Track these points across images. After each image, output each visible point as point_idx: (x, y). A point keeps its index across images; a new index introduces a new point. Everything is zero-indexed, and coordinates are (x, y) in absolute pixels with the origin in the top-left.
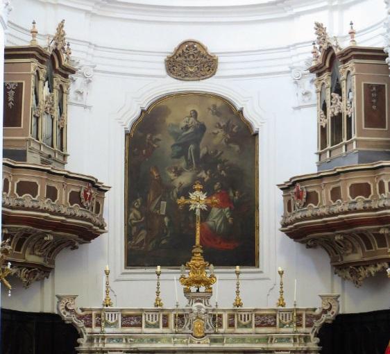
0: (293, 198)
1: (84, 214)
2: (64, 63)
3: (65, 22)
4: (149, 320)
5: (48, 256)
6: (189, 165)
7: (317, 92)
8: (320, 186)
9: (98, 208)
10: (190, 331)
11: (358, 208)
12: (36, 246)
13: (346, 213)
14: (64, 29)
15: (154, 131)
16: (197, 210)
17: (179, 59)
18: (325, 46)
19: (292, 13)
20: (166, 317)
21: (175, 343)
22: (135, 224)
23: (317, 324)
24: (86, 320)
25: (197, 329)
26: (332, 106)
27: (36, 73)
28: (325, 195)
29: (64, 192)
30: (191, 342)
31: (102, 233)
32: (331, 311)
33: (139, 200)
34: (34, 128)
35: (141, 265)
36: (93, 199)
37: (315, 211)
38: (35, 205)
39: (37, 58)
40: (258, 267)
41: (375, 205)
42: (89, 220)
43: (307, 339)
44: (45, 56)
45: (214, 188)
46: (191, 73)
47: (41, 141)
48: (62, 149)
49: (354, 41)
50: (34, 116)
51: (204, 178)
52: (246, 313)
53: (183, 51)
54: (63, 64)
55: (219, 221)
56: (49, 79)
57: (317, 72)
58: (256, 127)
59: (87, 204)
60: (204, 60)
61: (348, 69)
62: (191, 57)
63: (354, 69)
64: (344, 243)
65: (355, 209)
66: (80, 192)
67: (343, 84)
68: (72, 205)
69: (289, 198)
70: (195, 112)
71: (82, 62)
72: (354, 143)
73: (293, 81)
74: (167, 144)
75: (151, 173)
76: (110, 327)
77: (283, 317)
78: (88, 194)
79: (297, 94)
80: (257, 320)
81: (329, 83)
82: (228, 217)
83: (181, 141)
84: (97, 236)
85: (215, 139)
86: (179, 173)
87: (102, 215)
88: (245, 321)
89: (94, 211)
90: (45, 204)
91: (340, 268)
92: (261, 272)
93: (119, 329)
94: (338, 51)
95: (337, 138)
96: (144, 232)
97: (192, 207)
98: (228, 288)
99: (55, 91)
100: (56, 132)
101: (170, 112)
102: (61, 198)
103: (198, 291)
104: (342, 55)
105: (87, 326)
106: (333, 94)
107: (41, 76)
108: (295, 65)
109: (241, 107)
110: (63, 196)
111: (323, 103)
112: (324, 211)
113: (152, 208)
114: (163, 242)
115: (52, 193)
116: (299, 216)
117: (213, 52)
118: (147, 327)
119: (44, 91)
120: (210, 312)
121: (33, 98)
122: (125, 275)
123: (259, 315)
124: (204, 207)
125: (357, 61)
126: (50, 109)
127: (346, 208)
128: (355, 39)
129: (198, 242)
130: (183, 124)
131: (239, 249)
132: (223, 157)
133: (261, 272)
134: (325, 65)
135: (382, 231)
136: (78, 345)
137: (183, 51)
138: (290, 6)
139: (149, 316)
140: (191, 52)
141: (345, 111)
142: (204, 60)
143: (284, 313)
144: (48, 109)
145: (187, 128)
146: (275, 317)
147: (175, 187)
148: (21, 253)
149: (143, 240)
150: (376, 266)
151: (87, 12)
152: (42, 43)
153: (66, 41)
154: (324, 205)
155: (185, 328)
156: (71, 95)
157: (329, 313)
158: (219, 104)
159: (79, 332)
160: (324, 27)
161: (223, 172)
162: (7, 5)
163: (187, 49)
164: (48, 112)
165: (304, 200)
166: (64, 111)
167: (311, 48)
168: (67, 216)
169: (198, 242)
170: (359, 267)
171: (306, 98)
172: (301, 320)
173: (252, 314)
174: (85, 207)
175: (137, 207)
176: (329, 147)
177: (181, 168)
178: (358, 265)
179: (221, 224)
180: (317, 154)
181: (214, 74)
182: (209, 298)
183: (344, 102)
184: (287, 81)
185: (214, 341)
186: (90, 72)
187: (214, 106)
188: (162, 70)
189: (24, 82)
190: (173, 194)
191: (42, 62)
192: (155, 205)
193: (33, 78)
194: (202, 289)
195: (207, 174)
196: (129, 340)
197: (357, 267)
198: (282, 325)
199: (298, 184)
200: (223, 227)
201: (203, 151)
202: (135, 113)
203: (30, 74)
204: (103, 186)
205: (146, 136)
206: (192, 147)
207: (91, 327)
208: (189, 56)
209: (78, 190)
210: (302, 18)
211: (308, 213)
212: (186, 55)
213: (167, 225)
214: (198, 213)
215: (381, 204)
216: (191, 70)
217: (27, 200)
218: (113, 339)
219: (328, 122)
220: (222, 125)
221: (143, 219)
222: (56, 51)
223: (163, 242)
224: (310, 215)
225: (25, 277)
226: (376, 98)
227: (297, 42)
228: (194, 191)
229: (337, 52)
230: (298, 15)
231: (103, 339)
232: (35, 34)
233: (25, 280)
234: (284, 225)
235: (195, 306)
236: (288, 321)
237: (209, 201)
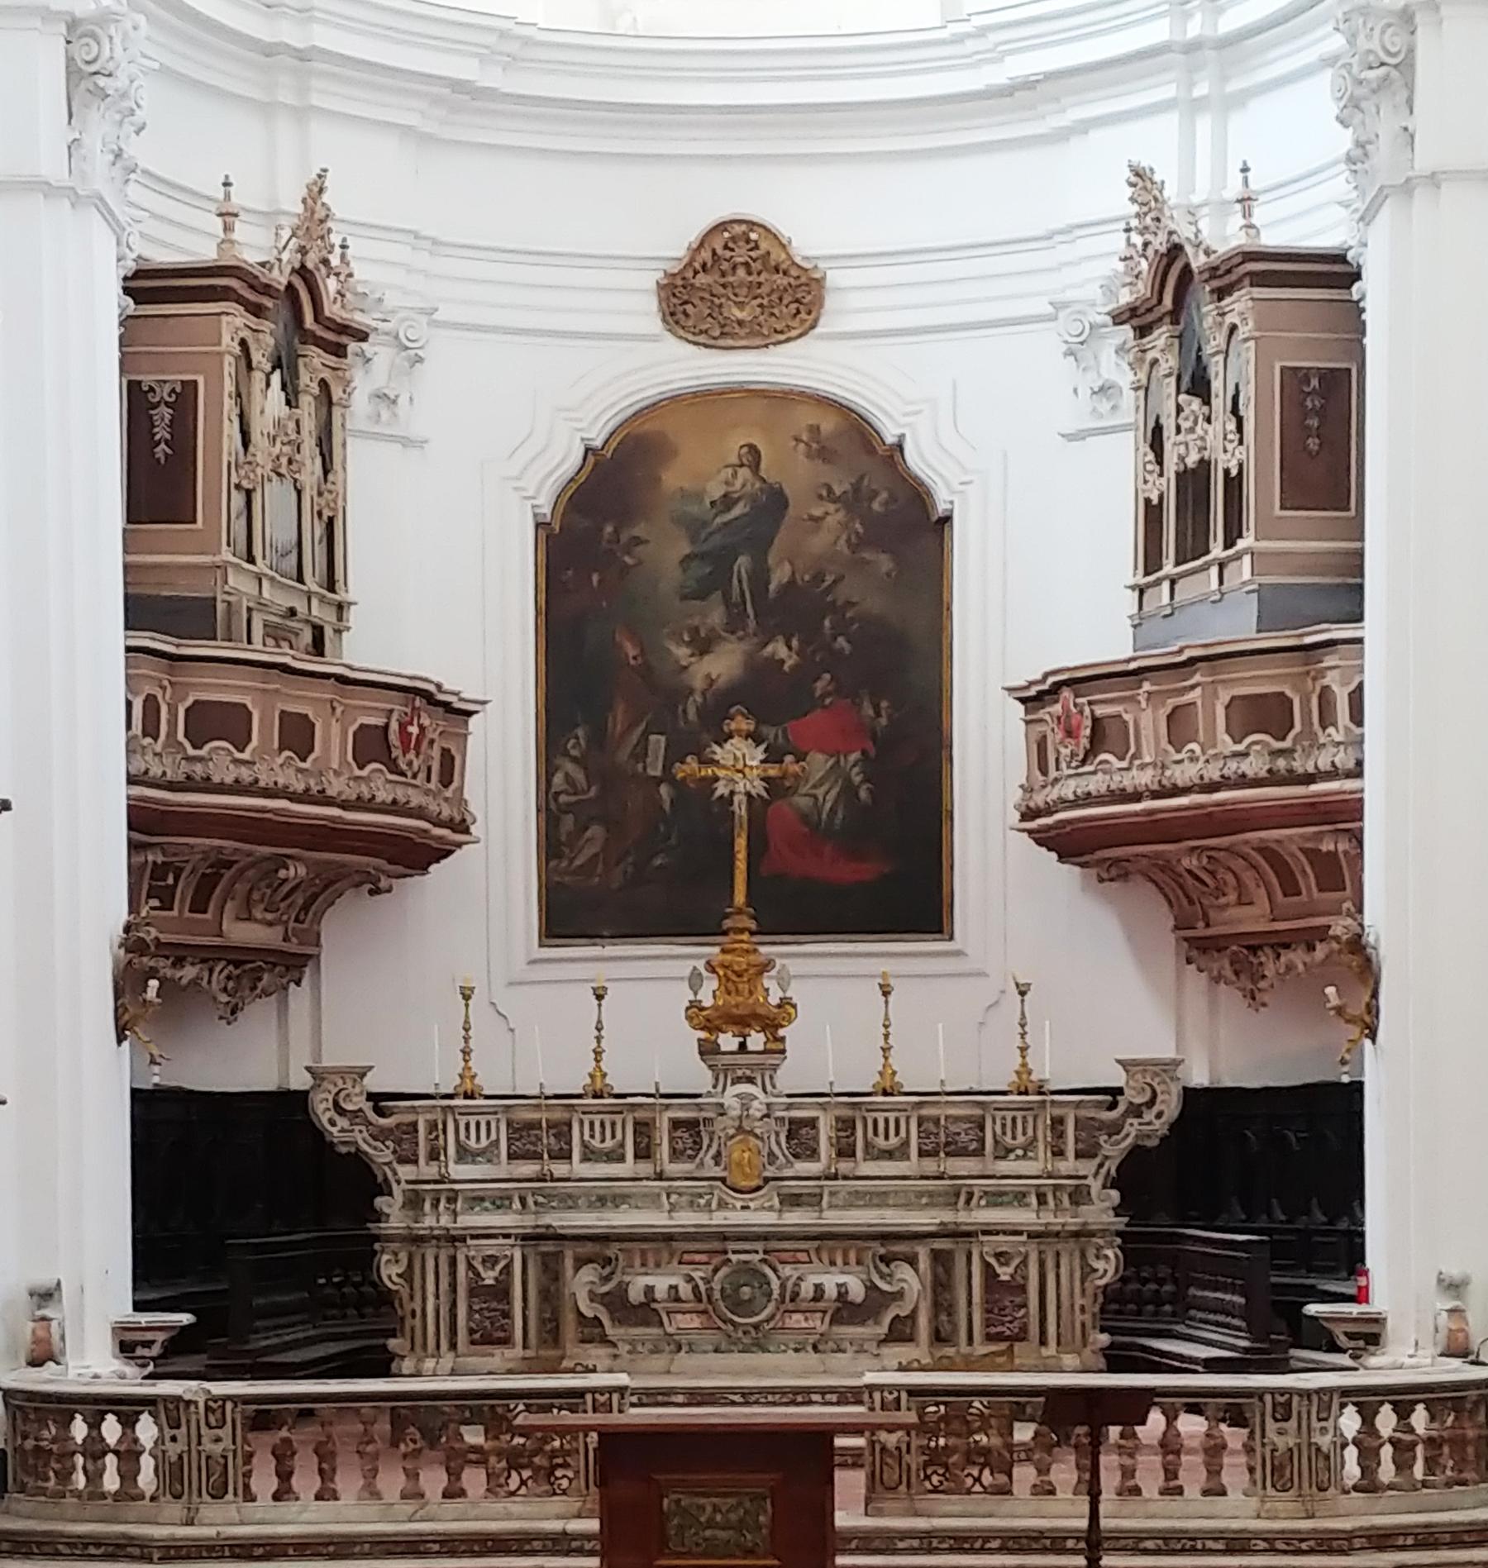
0: (1055, 736)
1: (400, 794)
2: (331, 310)
3: (329, 174)
4: (592, 1136)
5: (297, 920)
6: (735, 624)
7: (1136, 389)
8: (1133, 699)
9: (449, 769)
10: (718, 1172)
11: (1250, 773)
12: (256, 896)
13: (1212, 787)
14: (326, 198)
15: (625, 515)
16: (736, 799)
17: (702, 279)
18: (1160, 243)
19: (1063, 123)
20: (643, 1129)
21: (673, 1208)
22: (568, 809)
23: (1114, 1151)
24: (398, 1142)
25: (739, 1164)
26: (1181, 438)
27: (237, 350)
28: (1147, 721)
29: (336, 728)
30: (723, 1205)
31: (459, 845)
32: (1155, 1110)
33: (580, 732)
34: (240, 526)
35: (591, 935)
36: (432, 742)
37: (1117, 778)
38: (245, 774)
39: (240, 300)
40: (951, 938)
41: (1301, 765)
42: (419, 813)
43: (1079, 1196)
44: (267, 290)
45: (813, 691)
46: (740, 323)
47: (261, 566)
48: (331, 586)
49: (1250, 226)
50: (238, 487)
51: (783, 662)
52: (892, 1116)
53: (714, 253)
54: (327, 313)
55: (829, 796)
56: (285, 363)
57: (1136, 322)
58: (942, 500)
59: (410, 764)
60: (781, 281)
61: (1230, 319)
62: (741, 272)
63: (1251, 324)
64: (1212, 874)
65: (1244, 775)
66: (386, 727)
67: (1215, 366)
68: (361, 767)
69: (1040, 728)
70: (753, 449)
71: (392, 300)
72: (1247, 559)
73: (1064, 347)
74: (666, 553)
75: (620, 647)
76: (474, 1162)
77: (1004, 1126)
78: (414, 730)
79: (1075, 391)
80: (923, 1134)
81: (1169, 362)
82: (857, 779)
83: (705, 547)
84: (449, 853)
85: (816, 536)
86: (703, 646)
87: (461, 788)
88: (887, 1137)
89: (434, 777)
90: (279, 770)
91: (1201, 946)
92: (958, 953)
93: (503, 1169)
94: (1202, 259)
95: (1193, 547)
96: (595, 831)
97: (721, 789)
98: (843, 1013)
99: (306, 401)
100: (313, 531)
101: (675, 453)
102: (344, 733)
103: (743, 1046)
104: (1213, 272)
105: (402, 1161)
106: (1183, 397)
107: (257, 357)
108: (1070, 295)
109: (898, 432)
110: (333, 741)
111: (1151, 424)
112: (1144, 778)
113: (623, 755)
114: (658, 862)
115: (297, 735)
116: (1068, 790)
117: (810, 253)
118: (585, 1159)
119: (270, 403)
120: (779, 1114)
121: (232, 430)
122: (537, 967)
123: (929, 1119)
124: (758, 788)
125: (1258, 292)
126: (290, 462)
127: (1213, 773)
128: (1254, 221)
129: (740, 898)
130: (716, 491)
131: (894, 883)
132: (843, 593)
133: (958, 953)
134: (1160, 301)
135: (1327, 846)
136: (379, 1216)
137: (714, 253)
138: (1057, 100)
139: (592, 1124)
140: (741, 255)
141: (1222, 457)
142: (781, 281)
143: (1009, 1115)
144: (284, 460)
145: (728, 501)
146: (982, 1128)
147: (691, 691)
148: (208, 916)
149: (596, 855)
150: (1311, 948)
151: (406, 131)
152: (254, 246)
153: (335, 239)
154: (1147, 759)
155: (702, 1163)
156: (358, 408)
157: (1149, 1116)
158: (829, 424)
159: (380, 1179)
160: (1157, 178)
161: (841, 640)
162: (118, 155)
163: (726, 247)
164: (283, 470)
165: (1085, 742)
166: (337, 460)
167: (1118, 243)
168: (345, 805)
169: (740, 898)
170: (1260, 947)
171: (1105, 406)
172: (1061, 1135)
173: (908, 1118)
174: (403, 774)
175: (574, 753)
176: (1169, 568)
177: (713, 629)
178: (1254, 944)
179: (836, 802)
180: (1133, 588)
181: (813, 327)
182: (775, 1068)
183: (1217, 425)
184: (1048, 342)
185: (792, 1201)
186: (418, 330)
187: (815, 430)
188: (647, 314)
189: (201, 380)
190: (685, 711)
191: (257, 311)
192: (629, 750)
193: (229, 366)
194: (756, 1041)
195: (790, 648)
196: (530, 1201)
197: (1254, 949)
198: (1003, 1153)
199: (1066, 693)
200: (840, 815)
201: (780, 575)
202: (562, 461)
203: (219, 353)
204: (461, 700)
205: (601, 530)
206: (743, 562)
207: (416, 1162)
208: (734, 268)
209: (379, 721)
210: (1095, 135)
211: (1096, 784)
212: (725, 266)
213: (667, 806)
214: (740, 808)
215: (1324, 762)
216: (739, 314)
217: (219, 759)
218: (482, 1199)
219: (1165, 486)
220: (838, 491)
221: (593, 789)
222: (302, 271)
223: (658, 862)
224: (1103, 790)
225: (225, 990)
226: (1321, 413)
227: (1076, 221)
228: (723, 738)
229: (1198, 261)
230: (1084, 127)
231: (452, 1200)
232: (229, 219)
233: (224, 998)
234: (1028, 814)
235: (730, 1097)
236: (1021, 1139)
237: (773, 771)
